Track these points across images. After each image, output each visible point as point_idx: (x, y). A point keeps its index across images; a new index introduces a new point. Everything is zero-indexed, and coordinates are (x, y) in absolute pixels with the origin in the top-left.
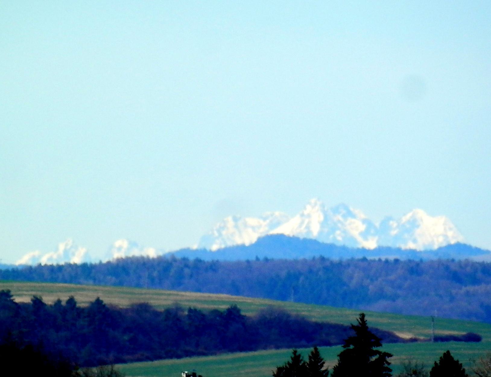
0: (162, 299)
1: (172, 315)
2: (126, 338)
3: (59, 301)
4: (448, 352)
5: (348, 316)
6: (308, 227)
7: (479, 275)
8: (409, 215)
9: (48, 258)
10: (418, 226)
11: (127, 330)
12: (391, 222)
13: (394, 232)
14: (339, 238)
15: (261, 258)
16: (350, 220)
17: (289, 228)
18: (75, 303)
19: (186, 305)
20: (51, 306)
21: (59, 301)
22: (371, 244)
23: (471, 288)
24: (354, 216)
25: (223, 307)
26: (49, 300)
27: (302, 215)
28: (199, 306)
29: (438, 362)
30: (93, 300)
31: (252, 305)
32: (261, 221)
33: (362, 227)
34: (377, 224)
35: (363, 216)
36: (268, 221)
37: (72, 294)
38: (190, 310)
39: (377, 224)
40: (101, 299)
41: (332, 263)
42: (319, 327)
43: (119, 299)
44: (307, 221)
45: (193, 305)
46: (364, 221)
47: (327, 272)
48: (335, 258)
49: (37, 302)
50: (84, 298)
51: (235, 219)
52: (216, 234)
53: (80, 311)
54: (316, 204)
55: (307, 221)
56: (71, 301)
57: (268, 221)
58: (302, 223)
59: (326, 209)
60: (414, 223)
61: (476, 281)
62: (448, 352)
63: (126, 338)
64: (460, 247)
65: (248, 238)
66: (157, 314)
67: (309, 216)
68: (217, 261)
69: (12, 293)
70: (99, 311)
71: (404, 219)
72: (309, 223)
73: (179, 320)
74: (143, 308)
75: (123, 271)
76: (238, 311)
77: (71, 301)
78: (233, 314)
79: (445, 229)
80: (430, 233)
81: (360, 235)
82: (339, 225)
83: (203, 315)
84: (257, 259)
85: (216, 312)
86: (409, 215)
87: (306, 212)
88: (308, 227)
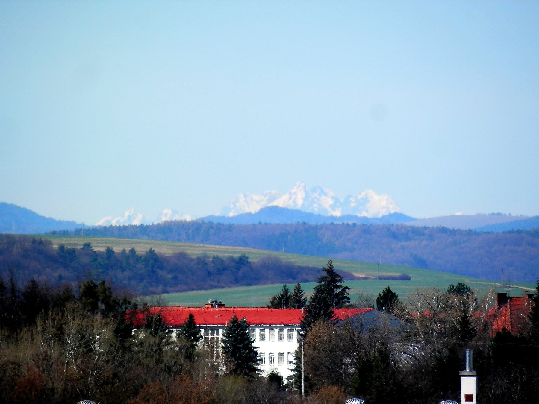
0: (195, 250)
1: (202, 261)
2: (170, 276)
3: (124, 250)
5: (322, 263)
6: (294, 201)
7: (410, 234)
8: (364, 193)
10: (369, 201)
11: (171, 271)
12: (351, 199)
13: (353, 205)
15: (263, 222)
16: (323, 197)
17: (280, 202)
18: (135, 252)
19: (211, 254)
20: (119, 253)
21: (124, 250)
22: (337, 213)
23: (405, 243)
24: (326, 194)
25: (236, 256)
26: (117, 249)
27: (290, 193)
28: (220, 255)
30: (148, 250)
31: (256, 255)
32: (263, 197)
33: (331, 202)
34: (342, 200)
35: (332, 194)
36: (267, 197)
37: (133, 245)
38: (214, 258)
39: (342, 200)
40: (153, 249)
41: (310, 226)
42: (301, 269)
43: (165, 249)
44: (293, 197)
45: (216, 254)
46: (333, 198)
47: (307, 232)
48: (313, 223)
49: (110, 251)
50: (141, 249)
51: (245, 196)
52: (232, 206)
53: (138, 259)
54: (300, 186)
55: (293, 197)
56: (132, 251)
57: (267, 197)
58: (290, 198)
59: (307, 189)
60: (366, 200)
61: (408, 239)
63: (170, 276)
64: (397, 215)
65: (254, 208)
66: (192, 260)
67: (295, 193)
68: (233, 224)
69: (92, 245)
71: (360, 197)
72: (295, 199)
73: (206, 264)
74: (182, 256)
75: (168, 230)
76: (247, 258)
77: (132, 251)
78: (242, 261)
79: (387, 204)
80: (378, 206)
81: (330, 206)
82: (316, 200)
83: (223, 261)
84: (260, 223)
85: (232, 259)
86: (364, 193)
87: (293, 191)
88: (294, 201)
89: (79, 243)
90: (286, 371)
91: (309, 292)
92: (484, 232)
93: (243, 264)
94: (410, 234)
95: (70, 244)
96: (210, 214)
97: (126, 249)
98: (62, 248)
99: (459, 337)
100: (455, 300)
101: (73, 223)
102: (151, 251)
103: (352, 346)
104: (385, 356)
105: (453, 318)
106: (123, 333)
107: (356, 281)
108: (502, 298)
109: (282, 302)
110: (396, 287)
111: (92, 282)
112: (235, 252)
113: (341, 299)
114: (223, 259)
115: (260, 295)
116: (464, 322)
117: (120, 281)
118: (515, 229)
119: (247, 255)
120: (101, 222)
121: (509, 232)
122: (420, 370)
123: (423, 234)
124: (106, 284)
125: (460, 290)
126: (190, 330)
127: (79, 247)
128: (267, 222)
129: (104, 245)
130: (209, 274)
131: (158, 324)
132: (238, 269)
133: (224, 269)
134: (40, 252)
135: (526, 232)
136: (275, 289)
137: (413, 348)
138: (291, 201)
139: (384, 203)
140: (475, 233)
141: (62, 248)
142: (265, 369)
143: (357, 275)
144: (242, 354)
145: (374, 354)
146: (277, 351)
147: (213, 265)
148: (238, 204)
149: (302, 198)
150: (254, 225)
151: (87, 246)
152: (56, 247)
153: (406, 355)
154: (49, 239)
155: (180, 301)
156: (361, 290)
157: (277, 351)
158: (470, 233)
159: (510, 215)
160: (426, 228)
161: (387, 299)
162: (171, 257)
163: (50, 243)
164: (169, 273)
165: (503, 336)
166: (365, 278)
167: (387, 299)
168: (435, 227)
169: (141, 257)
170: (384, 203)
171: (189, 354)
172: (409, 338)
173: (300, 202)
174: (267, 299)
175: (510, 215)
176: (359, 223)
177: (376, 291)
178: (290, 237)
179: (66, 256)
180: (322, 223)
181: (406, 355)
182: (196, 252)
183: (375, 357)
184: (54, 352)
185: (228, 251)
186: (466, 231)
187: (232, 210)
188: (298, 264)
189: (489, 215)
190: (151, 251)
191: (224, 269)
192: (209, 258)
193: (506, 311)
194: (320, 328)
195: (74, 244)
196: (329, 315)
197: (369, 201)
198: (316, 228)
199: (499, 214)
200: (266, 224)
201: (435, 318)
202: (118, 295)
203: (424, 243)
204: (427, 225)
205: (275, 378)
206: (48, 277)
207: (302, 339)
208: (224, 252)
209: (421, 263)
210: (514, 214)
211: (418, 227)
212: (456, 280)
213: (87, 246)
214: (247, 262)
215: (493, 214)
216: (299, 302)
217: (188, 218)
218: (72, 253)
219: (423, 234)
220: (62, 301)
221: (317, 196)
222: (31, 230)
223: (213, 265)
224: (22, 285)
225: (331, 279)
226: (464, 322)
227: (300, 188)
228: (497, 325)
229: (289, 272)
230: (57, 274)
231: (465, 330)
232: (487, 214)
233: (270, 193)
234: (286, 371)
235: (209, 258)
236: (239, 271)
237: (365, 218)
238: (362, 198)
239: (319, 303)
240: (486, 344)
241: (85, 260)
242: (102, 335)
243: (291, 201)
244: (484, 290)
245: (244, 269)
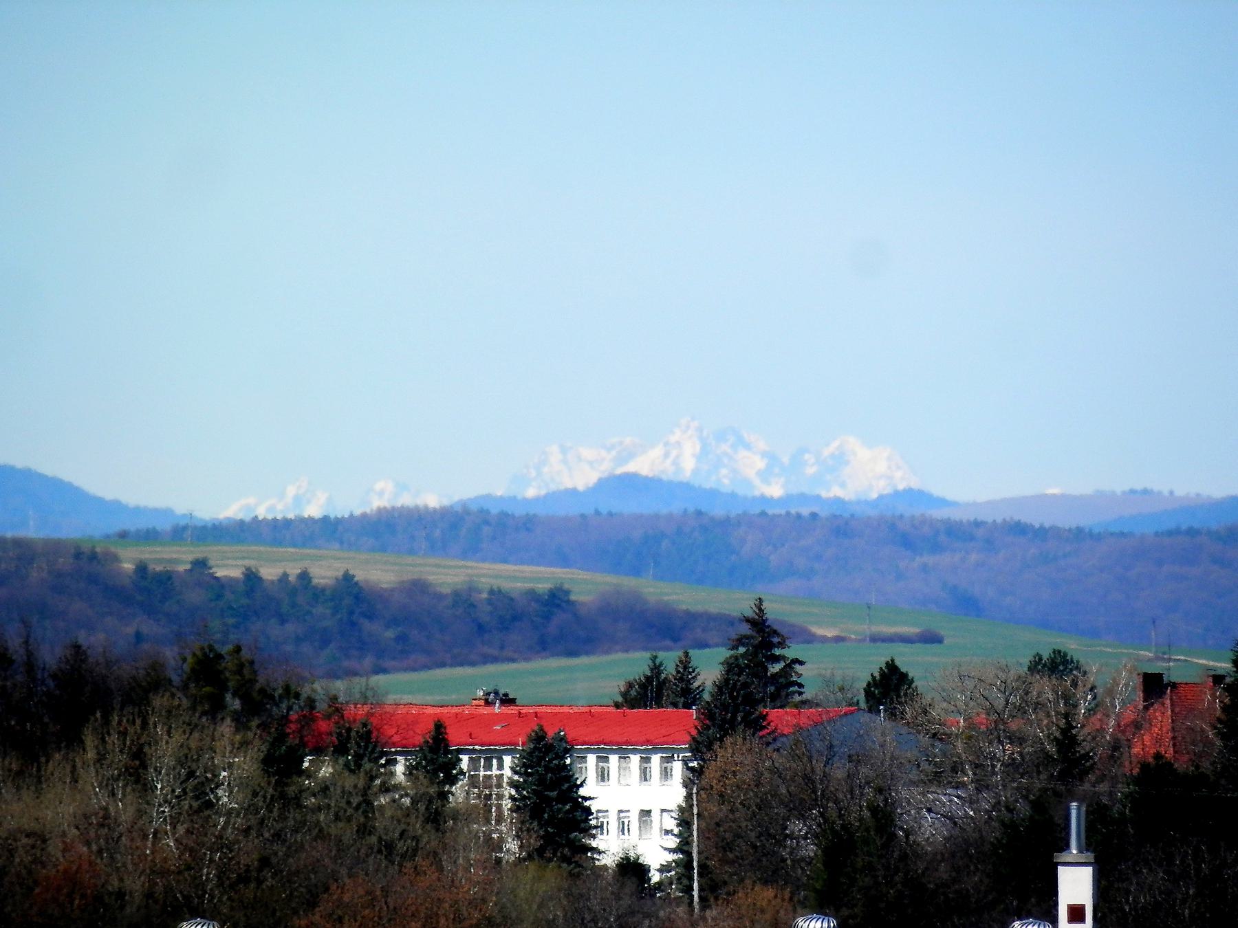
0: (448, 574)
1: (463, 600)
2: (390, 634)
3: (285, 575)
5: (739, 603)
6: (675, 463)
7: (942, 538)
8: (836, 444)
10: (847, 463)
11: (393, 622)
12: (807, 456)
13: (811, 470)
15: (604, 511)
16: (742, 453)
17: (643, 465)
18: (310, 580)
19: (485, 583)
20: (272, 582)
21: (285, 575)
22: (775, 490)
23: (929, 559)
24: (748, 447)
25: (543, 587)
26: (269, 573)
27: (666, 444)
28: (506, 585)
30: (340, 574)
31: (587, 585)
32: (603, 453)
33: (760, 464)
34: (786, 460)
35: (762, 445)
36: (614, 453)
37: (306, 564)
38: (491, 592)
39: (786, 460)
40: (351, 572)
41: (712, 519)
42: (692, 618)
43: (379, 572)
44: (674, 453)
45: (496, 583)
46: (764, 454)
47: (705, 533)
48: (718, 511)
49: (252, 577)
50: (325, 572)
51: (564, 450)
52: (533, 474)
53: (317, 594)
54: (688, 427)
55: (674, 453)
56: (304, 576)
57: (614, 453)
58: (667, 455)
59: (705, 433)
60: (840, 459)
61: (936, 548)
63: (390, 634)
64: (912, 495)
65: (583, 478)
66: (440, 597)
67: (678, 443)
68: (535, 515)
69: (211, 563)
71: (826, 452)
72: (677, 457)
73: (473, 605)
74: (418, 587)
75: (386, 529)
76: (567, 592)
77: (304, 576)
78: (556, 600)
79: (889, 468)
80: (867, 473)
81: (758, 473)
82: (726, 460)
83: (512, 599)
84: (597, 513)
85: (532, 595)
86: (836, 444)
87: (673, 439)
88: (675, 463)
89: (181, 558)
90: (656, 852)
91: (709, 670)
92: (1112, 534)
93: (558, 606)
94: (942, 538)
95: (160, 561)
96: (483, 491)
97: (289, 571)
98: (142, 569)
99: (1055, 775)
100: (1045, 688)
101: (168, 512)
102: (348, 577)
103: (809, 794)
104: (884, 817)
105: (1041, 730)
106: (282, 764)
107: (817, 646)
108: (1154, 685)
109: (647, 693)
110: (910, 660)
111: (211, 648)
112: (539, 580)
113: (784, 687)
114: (513, 596)
115: (598, 678)
116: (1067, 740)
117: (277, 645)
118: (1184, 527)
119: (566, 586)
120: (231, 509)
121: (1170, 533)
122: (964, 849)
123: (972, 538)
124: (243, 652)
125: (1057, 665)
126: (437, 758)
127: (182, 568)
128: (614, 511)
129: (240, 562)
130: (481, 628)
131: (362, 744)
132: (547, 617)
133: (515, 618)
134: (93, 579)
135: (1209, 533)
136: (632, 665)
137: (949, 800)
138: (669, 461)
139: (882, 467)
140: (1091, 535)
141: (142, 569)
142: (609, 847)
143: (819, 631)
144: (557, 814)
145: (858, 813)
146: (637, 806)
147: (489, 608)
148: (546, 469)
149: (694, 455)
150: (583, 516)
151: (201, 564)
152: (128, 566)
153: (933, 816)
154: (113, 549)
155: (413, 692)
156: (830, 665)
157: (637, 806)
158: (1079, 534)
159: (1171, 493)
160: (978, 524)
161: (890, 687)
162: (393, 590)
163: (116, 558)
164: (387, 626)
165: (1155, 773)
166: (838, 639)
167: (890, 687)
168: (999, 520)
169: (323, 590)
170: (882, 467)
171: (435, 813)
172: (940, 776)
173: (688, 465)
174: (612, 688)
175: (1171, 493)
176: (824, 513)
177: (863, 668)
178: (665, 544)
179: (153, 588)
180: (740, 512)
181: (933, 816)
182: (449, 580)
183: (861, 820)
184: (123, 808)
185: (523, 576)
186: (1070, 530)
187: (534, 483)
188: (684, 607)
189: (1124, 493)
190: (348, 577)
191: (515, 618)
192: (480, 592)
193: (1162, 715)
194: (735, 753)
195: (171, 561)
196: (756, 724)
197: (847, 463)
198: (726, 523)
199: (1145, 492)
200: (610, 514)
201: (999, 731)
202: (272, 677)
203: (974, 557)
204: (981, 517)
205: (632, 869)
206: (111, 637)
207: (694, 778)
208: (515, 579)
209: (967, 605)
210: (1180, 492)
211: (961, 522)
212: (1046, 643)
213: (201, 564)
214: (568, 602)
215: (1133, 492)
216: (686, 694)
217: (432, 500)
218: (165, 581)
219: (972, 538)
220: (142, 690)
221: (729, 451)
222: (72, 528)
223: (489, 608)
224: (51, 655)
225: (761, 640)
226: (1067, 740)
227: (690, 432)
228: (1142, 747)
229: (663, 626)
230: (130, 630)
231: (1069, 759)
232: (1119, 492)
233: (621, 443)
234: (656, 852)
235: (480, 592)
236: (549, 623)
237: (838, 501)
238: (832, 456)
239: (733, 696)
240: (1116, 791)
241: (195, 597)
242: (235, 769)
243: (669, 461)
244: (1111, 666)
245: (559, 618)
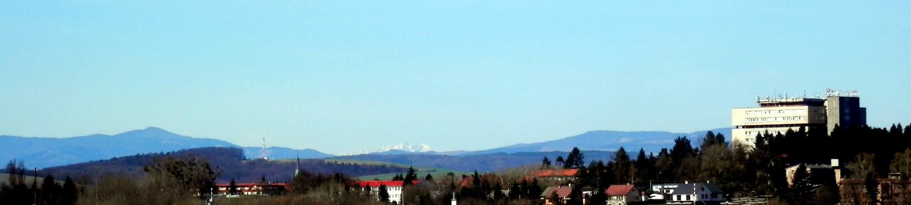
0: (369, 163)
1: (371, 166)
4: (622, 150)
5: (408, 166)
9: (345, 154)
14: (410, 148)
17: (395, 148)
29: (903, 127)
31: (388, 164)
43: (359, 163)
47: (404, 157)
50: (352, 163)
60: (422, 147)
62: (622, 150)
65: (387, 150)
70: (356, 166)
74: (365, 165)
75: (361, 157)
78: (384, 166)
80: (426, 148)
81: (411, 149)
89: (333, 161)
90: (398, 200)
91: (404, 176)
99: (451, 188)
100: (450, 177)
103: (418, 192)
104: (428, 195)
105: (449, 183)
106: (347, 189)
108: (464, 176)
109: (396, 179)
110: (432, 174)
113: (415, 178)
115: (390, 176)
116: (453, 184)
117: (346, 173)
120: (340, 155)
122: (439, 199)
125: (451, 174)
126: (368, 188)
131: (358, 186)
136: (394, 175)
137: (437, 192)
142: (391, 199)
144: (384, 195)
145: (425, 194)
146: (395, 194)
153: (435, 194)
155: (365, 179)
156: (421, 174)
157: (395, 194)
161: (429, 177)
165: (464, 188)
167: (429, 177)
171: (368, 195)
172: (436, 189)
174: (391, 178)
175: (642, 153)
177: (425, 175)
179: (330, 164)
181: (435, 194)
183: (576, 176)
184: (326, 195)
185: (379, 163)
193: (465, 181)
194: (408, 187)
196: (411, 183)
201: (444, 183)
202: (346, 177)
205: (395, 202)
206: (323, 172)
207: (403, 190)
209: (439, 166)
212: (449, 171)
216: (402, 179)
220: (329, 179)
222: (319, 157)
224: (316, 174)
225: (411, 171)
226: (453, 184)
228: (463, 185)
229: (399, 169)
231: (453, 187)
234: (398, 200)
236: (383, 169)
239: (408, 179)
240: (459, 191)
242: (341, 189)
244: (458, 174)
